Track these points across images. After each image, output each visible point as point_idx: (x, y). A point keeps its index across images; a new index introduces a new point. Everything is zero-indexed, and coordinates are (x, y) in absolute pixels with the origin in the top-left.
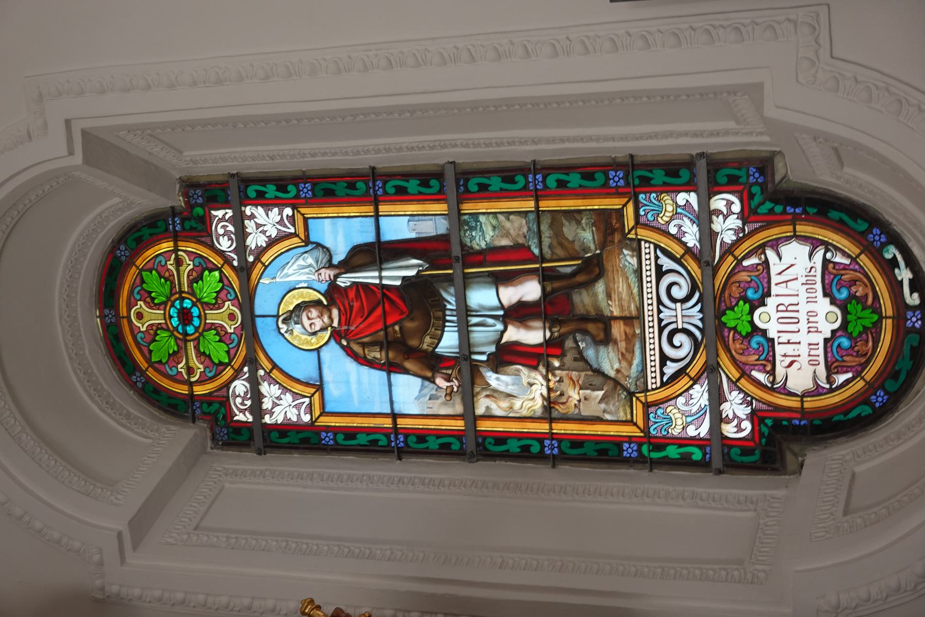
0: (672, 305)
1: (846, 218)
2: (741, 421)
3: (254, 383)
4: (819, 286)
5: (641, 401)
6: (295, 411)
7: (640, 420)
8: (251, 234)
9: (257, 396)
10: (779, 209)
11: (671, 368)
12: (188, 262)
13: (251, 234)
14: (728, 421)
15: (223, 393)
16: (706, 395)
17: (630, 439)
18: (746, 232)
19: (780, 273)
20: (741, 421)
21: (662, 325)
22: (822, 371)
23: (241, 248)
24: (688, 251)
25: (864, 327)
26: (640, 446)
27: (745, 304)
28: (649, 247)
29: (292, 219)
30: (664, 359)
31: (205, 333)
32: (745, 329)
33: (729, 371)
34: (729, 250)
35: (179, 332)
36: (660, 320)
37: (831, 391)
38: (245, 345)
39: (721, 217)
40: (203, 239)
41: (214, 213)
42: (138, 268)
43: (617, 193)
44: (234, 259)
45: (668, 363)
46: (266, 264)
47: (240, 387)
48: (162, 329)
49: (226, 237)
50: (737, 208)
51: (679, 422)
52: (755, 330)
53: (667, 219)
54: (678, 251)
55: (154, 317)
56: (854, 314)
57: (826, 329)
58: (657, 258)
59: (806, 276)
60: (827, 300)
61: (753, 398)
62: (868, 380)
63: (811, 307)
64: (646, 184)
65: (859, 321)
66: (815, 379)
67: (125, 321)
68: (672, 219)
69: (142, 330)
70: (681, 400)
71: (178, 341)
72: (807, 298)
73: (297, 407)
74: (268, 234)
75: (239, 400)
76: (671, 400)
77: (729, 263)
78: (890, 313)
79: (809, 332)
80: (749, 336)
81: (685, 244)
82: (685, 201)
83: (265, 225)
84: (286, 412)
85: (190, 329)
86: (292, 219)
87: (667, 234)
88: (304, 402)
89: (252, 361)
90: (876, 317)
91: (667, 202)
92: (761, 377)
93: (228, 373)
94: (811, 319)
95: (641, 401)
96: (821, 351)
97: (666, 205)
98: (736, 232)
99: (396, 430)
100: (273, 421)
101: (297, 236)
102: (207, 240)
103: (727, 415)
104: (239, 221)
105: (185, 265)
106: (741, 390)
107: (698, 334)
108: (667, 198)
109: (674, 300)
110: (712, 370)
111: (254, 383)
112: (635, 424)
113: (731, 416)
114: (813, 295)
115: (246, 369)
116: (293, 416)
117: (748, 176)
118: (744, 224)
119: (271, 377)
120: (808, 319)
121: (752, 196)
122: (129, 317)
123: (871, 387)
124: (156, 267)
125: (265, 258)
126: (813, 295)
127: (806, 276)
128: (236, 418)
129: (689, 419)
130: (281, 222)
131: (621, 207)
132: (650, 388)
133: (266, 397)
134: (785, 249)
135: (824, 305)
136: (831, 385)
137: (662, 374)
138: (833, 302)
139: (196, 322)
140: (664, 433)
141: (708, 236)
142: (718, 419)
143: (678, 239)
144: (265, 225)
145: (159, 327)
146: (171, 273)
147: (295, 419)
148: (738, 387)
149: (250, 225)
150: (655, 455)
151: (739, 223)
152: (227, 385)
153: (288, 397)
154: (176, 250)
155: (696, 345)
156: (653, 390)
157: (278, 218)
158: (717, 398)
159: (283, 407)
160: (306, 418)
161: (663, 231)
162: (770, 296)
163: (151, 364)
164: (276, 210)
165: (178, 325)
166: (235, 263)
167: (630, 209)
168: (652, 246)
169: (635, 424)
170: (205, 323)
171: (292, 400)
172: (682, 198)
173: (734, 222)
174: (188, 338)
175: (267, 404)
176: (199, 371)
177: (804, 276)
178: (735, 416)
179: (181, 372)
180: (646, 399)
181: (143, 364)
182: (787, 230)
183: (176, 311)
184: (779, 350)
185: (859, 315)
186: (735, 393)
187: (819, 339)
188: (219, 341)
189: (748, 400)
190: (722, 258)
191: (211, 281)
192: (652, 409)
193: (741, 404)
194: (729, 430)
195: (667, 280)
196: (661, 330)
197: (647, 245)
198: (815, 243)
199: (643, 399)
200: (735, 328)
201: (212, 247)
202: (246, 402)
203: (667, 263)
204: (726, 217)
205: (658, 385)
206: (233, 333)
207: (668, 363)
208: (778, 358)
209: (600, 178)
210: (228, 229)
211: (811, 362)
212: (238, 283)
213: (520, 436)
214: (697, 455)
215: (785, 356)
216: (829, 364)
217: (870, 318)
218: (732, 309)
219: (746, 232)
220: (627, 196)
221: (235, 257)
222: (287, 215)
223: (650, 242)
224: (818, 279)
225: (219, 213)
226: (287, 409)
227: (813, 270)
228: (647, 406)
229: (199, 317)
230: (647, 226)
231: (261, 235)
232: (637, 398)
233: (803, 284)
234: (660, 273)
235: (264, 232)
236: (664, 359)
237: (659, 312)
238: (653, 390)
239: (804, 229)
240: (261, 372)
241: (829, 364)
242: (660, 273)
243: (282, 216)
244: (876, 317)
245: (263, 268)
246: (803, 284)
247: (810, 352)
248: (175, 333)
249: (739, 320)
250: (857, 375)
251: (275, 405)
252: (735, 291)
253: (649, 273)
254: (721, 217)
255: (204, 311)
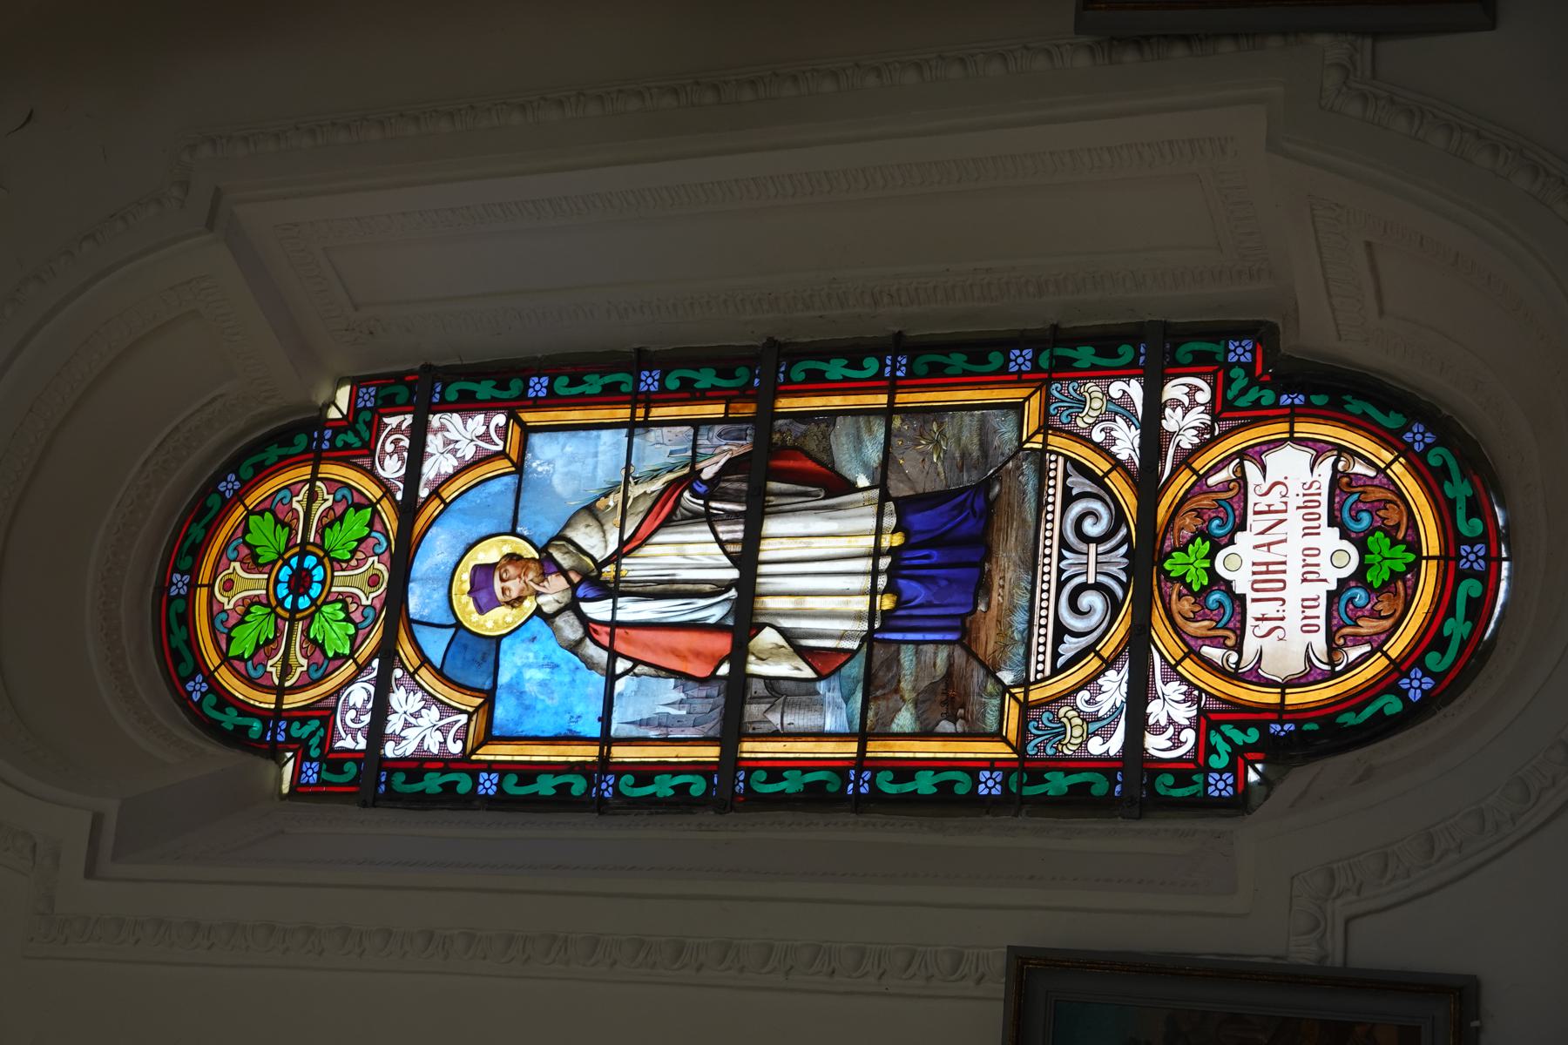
0: (1083, 547)
1: (1373, 412)
2: (1179, 729)
3: (383, 688)
4: (1323, 510)
5: (1017, 700)
6: (439, 736)
7: (1012, 727)
8: (432, 455)
9: (381, 709)
10: (1268, 397)
11: (1070, 646)
12: (326, 497)
13: (432, 455)
14: (1159, 730)
15: (331, 702)
16: (1124, 688)
17: (992, 764)
18: (1217, 433)
19: (1262, 533)
20: (1179, 729)
21: (1063, 578)
22: (1319, 642)
23: (412, 476)
24: (1117, 464)
25: (1392, 571)
26: (1007, 776)
27: (1203, 542)
28: (1056, 461)
29: (503, 432)
30: (1061, 631)
31: (326, 547)
32: (1198, 580)
33: (1164, 641)
34: (1185, 459)
35: (284, 608)
36: (1060, 571)
37: (1334, 675)
38: (381, 628)
39: (1179, 410)
40: (359, 461)
41: (386, 420)
42: (246, 508)
43: (1019, 380)
44: (399, 489)
45: (1067, 638)
46: (448, 501)
47: (359, 694)
48: (260, 603)
49: (395, 457)
50: (1204, 397)
51: (1077, 732)
52: (1216, 581)
53: (1091, 421)
54: (1100, 465)
55: (251, 584)
56: (1376, 553)
57: (1332, 577)
58: (1066, 475)
59: (1304, 495)
60: (1336, 531)
61: (1201, 690)
62: (1394, 657)
63: (1311, 541)
64: (1065, 369)
65: (1387, 563)
66: (1308, 648)
67: (205, 591)
68: (1097, 421)
69: (226, 607)
70: (1084, 695)
71: (279, 620)
72: (1304, 529)
73: (444, 730)
74: (459, 455)
75: (352, 714)
76: (1064, 697)
77: (1185, 480)
78: (1435, 551)
79: (1304, 580)
80: (1205, 591)
81: (1113, 456)
82: (1121, 392)
83: (457, 442)
84: (424, 737)
85: (304, 602)
86: (503, 432)
87: (1087, 441)
88: (456, 722)
89: (387, 653)
90: (1411, 557)
91: (1093, 395)
92: (1214, 653)
93: (349, 668)
94: (1310, 560)
95: (1017, 700)
96: (1321, 611)
97: (1091, 399)
98: (1200, 431)
99: (604, 763)
100: (399, 753)
101: (507, 457)
102: (366, 462)
103: (1158, 721)
104: (419, 434)
105: (319, 501)
106: (1183, 680)
107: (1119, 592)
108: (1092, 387)
109: (1087, 540)
110: (1138, 647)
111: (383, 688)
112: (1005, 740)
113: (1163, 722)
114: (1315, 524)
115: (375, 663)
116: (433, 745)
117: (1228, 351)
118: (1213, 421)
119: (415, 680)
120: (1304, 560)
121: (1229, 382)
122: (211, 586)
123: (1398, 668)
124: (271, 508)
125: (449, 493)
126: (1315, 524)
127: (1304, 495)
128: (339, 744)
129: (1093, 727)
130: (485, 437)
131: (1021, 400)
132: (1032, 679)
133: (396, 712)
134: (1272, 459)
135: (1330, 538)
136: (1333, 668)
137: (1056, 655)
138: (1344, 535)
139: (315, 590)
140: (1050, 752)
141: (1153, 438)
142: (1138, 724)
143: (1102, 450)
144: (457, 442)
145: (255, 601)
146: (295, 515)
147: (435, 750)
148: (1179, 674)
149: (434, 443)
150: (1029, 791)
151: (1207, 418)
152: (337, 692)
153: (434, 713)
154: (314, 477)
155: (1114, 606)
156: (1037, 681)
157: (482, 430)
158: (1140, 693)
159: (422, 729)
160: (455, 748)
161: (1083, 438)
162: (1244, 529)
163: (226, 659)
164: (480, 418)
165: (287, 596)
166: (399, 496)
167: (1035, 402)
168: (1061, 460)
169: (1005, 740)
170: (329, 592)
171: (438, 719)
172: (1116, 389)
173: (1197, 417)
174: (298, 616)
175: (394, 724)
176: (299, 670)
177: (1301, 495)
178: (1171, 721)
179: (271, 673)
180: (1026, 695)
181: (212, 659)
182: (1279, 429)
183: (290, 572)
184: (1253, 610)
185: (1386, 553)
186: (1174, 685)
187: (1320, 590)
188: (344, 620)
189: (1193, 693)
190: (1175, 471)
191: (356, 524)
192: (1033, 713)
193: (1185, 701)
194: (1155, 744)
195: (1077, 508)
196: (1061, 585)
197: (1053, 458)
198: (1319, 448)
199: (1021, 697)
200: (1182, 579)
201: (371, 474)
202: (362, 718)
203: (1079, 484)
204: (1186, 410)
205: (1048, 672)
206: (371, 606)
207: (1067, 638)
208: (1250, 622)
209: (996, 359)
210: (402, 444)
211: (1305, 628)
212: (395, 525)
213: (806, 766)
214: (1100, 787)
215: (1263, 619)
216: (1335, 629)
217: (1400, 558)
218: (1184, 549)
219: (1217, 433)
220: (1032, 385)
221: (401, 486)
222: (497, 425)
223: (1058, 454)
224: (1324, 499)
225: (392, 421)
226: (428, 732)
227: (1316, 485)
228: (1025, 707)
229: (323, 582)
230: (1058, 431)
231: (449, 456)
232: (1013, 696)
233: (1298, 508)
234: (1069, 499)
235: (454, 452)
236: (1061, 631)
237: (1061, 558)
238: (1037, 681)
239: (1304, 429)
240: (398, 673)
241: (1335, 629)
242: (1069, 499)
243: (488, 427)
244: (1411, 557)
245: (442, 506)
246: (1298, 508)
247: (1303, 612)
248: (279, 610)
249: (1191, 566)
250: (1378, 649)
251: (407, 725)
252: (1188, 523)
253: (1055, 496)
254: (1179, 410)
255: (333, 571)
